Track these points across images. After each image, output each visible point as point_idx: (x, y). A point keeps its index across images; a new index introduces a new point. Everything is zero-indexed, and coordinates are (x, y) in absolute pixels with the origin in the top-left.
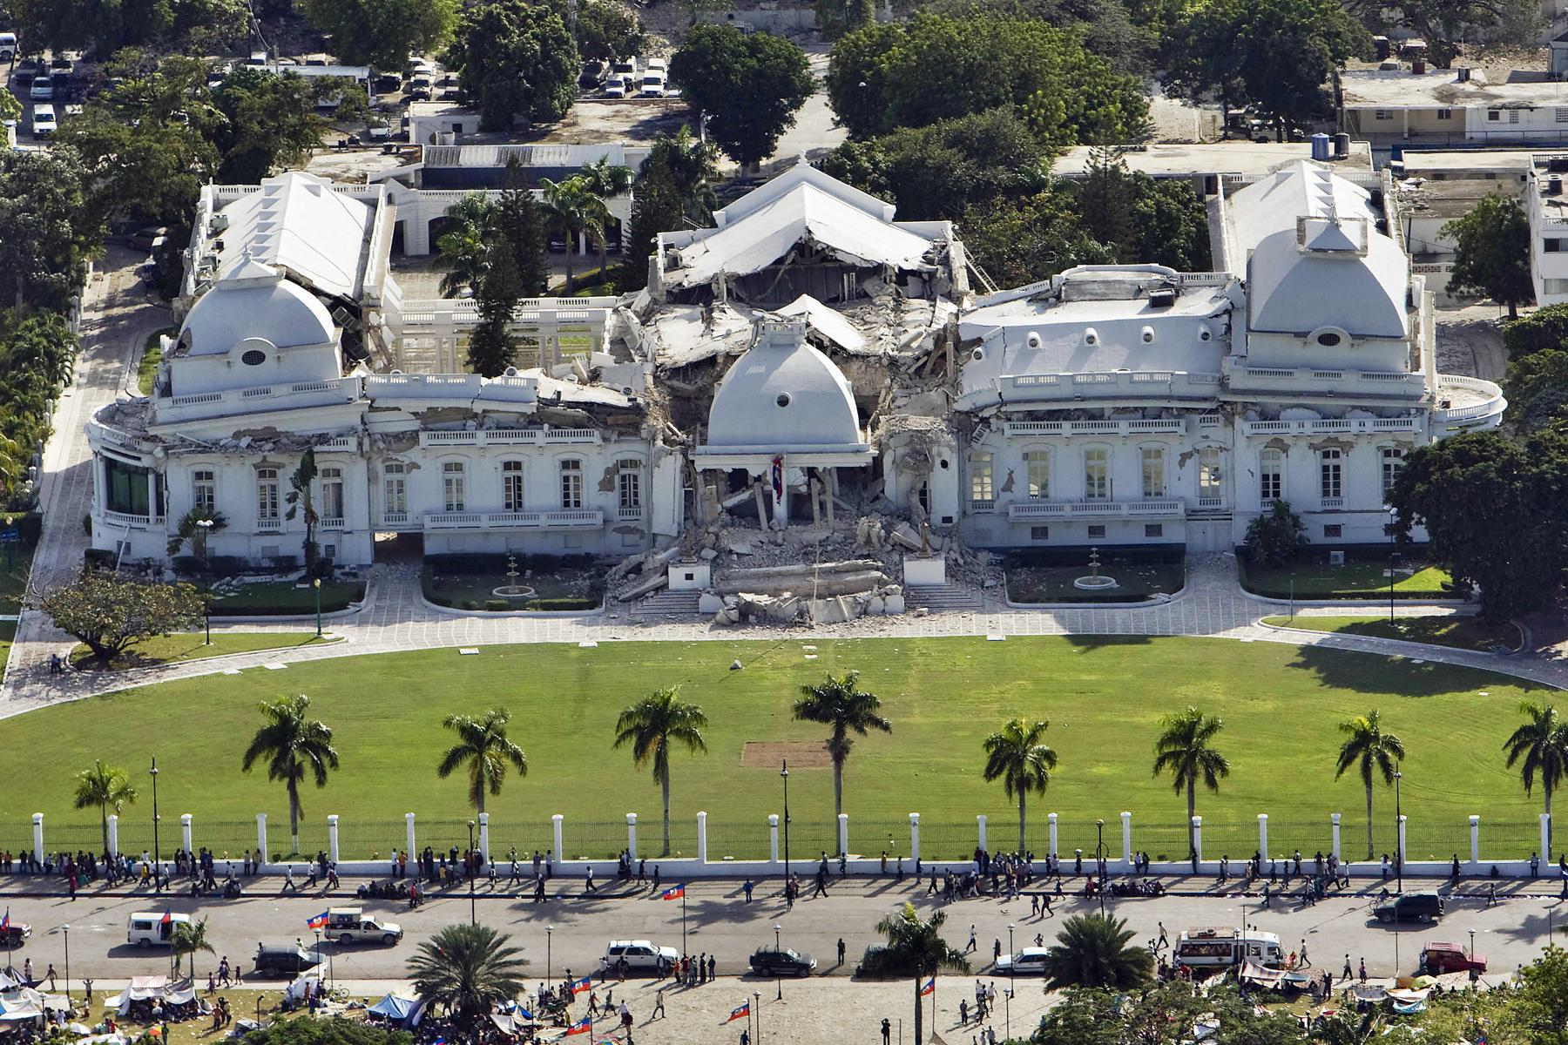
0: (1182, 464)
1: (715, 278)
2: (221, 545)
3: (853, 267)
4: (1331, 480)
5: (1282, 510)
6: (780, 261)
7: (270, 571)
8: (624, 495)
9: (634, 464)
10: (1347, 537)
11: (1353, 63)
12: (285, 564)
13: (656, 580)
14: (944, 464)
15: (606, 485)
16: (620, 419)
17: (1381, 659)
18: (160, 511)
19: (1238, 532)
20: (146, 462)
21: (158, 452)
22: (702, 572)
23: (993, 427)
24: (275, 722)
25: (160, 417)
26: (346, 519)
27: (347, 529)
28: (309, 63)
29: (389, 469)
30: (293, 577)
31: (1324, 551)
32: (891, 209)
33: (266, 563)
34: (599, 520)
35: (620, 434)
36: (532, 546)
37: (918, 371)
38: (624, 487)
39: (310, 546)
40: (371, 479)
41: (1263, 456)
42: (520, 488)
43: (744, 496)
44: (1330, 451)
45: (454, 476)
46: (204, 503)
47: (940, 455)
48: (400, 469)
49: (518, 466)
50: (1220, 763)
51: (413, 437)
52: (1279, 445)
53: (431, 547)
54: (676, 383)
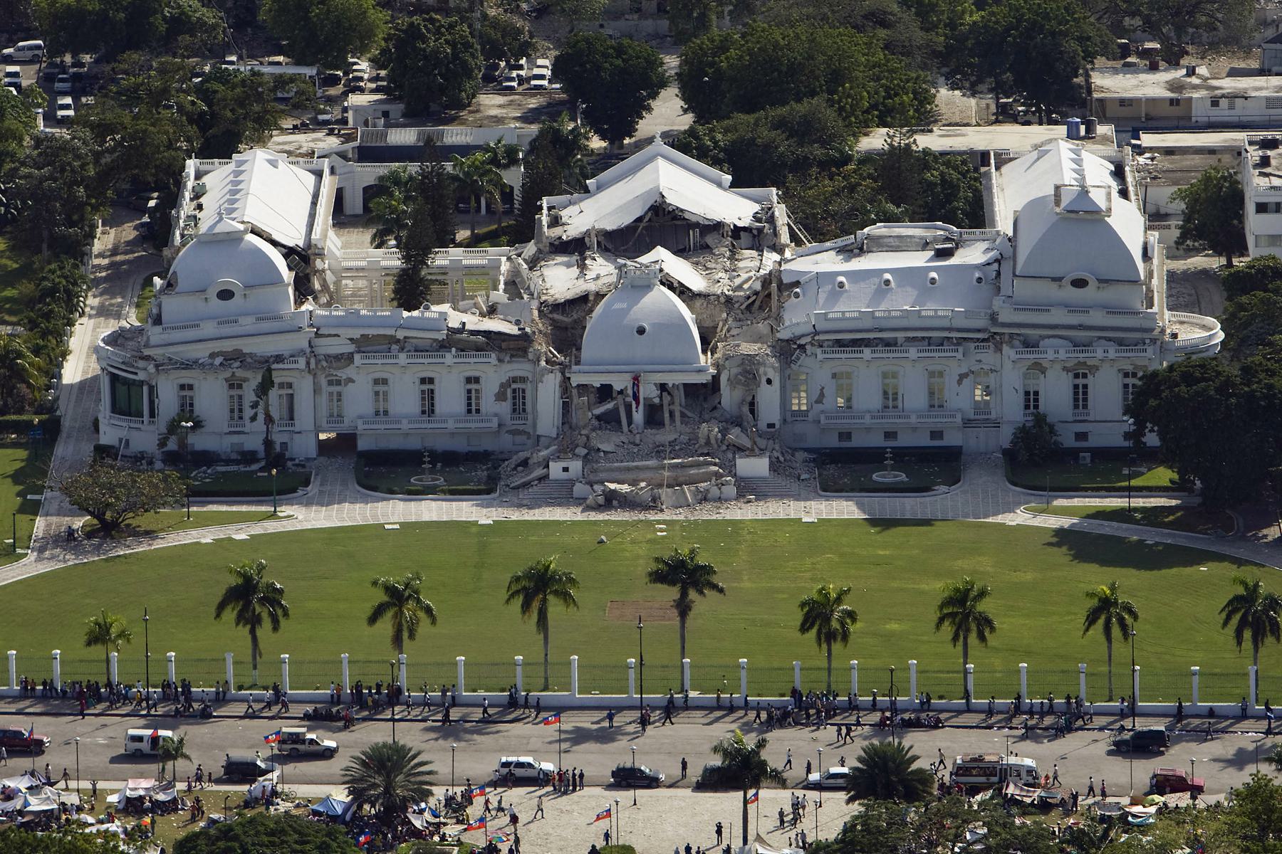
0: (960, 382)
1: (588, 233)
2: (199, 442)
3: (697, 225)
4: (1080, 396)
5: (1040, 419)
6: (639, 220)
7: (237, 462)
8: (514, 404)
9: (523, 380)
10: (1093, 442)
11: (1100, 61)
12: (248, 457)
13: (539, 472)
14: (769, 382)
15: (500, 396)
16: (512, 344)
17: (1120, 540)
18: (152, 414)
19: (1005, 437)
20: (141, 376)
21: (151, 369)
22: (576, 466)
23: (809, 352)
24: (240, 581)
25: (153, 341)
26: (296, 422)
27: (297, 429)
28: (271, 64)
29: (330, 383)
30: (255, 467)
31: (1074, 453)
32: (728, 178)
33: (234, 456)
34: (495, 423)
35: (512, 356)
36: (442, 444)
37: (749, 307)
38: (514, 398)
39: (268, 443)
40: (317, 390)
41: (1026, 376)
42: (432, 398)
43: (610, 406)
44: (1080, 373)
45: (381, 388)
46: (187, 409)
47: (765, 374)
48: (339, 383)
49: (431, 381)
50: (989, 622)
51: (349, 358)
52: (1039, 368)
53: (362, 445)
54: (556, 316)
